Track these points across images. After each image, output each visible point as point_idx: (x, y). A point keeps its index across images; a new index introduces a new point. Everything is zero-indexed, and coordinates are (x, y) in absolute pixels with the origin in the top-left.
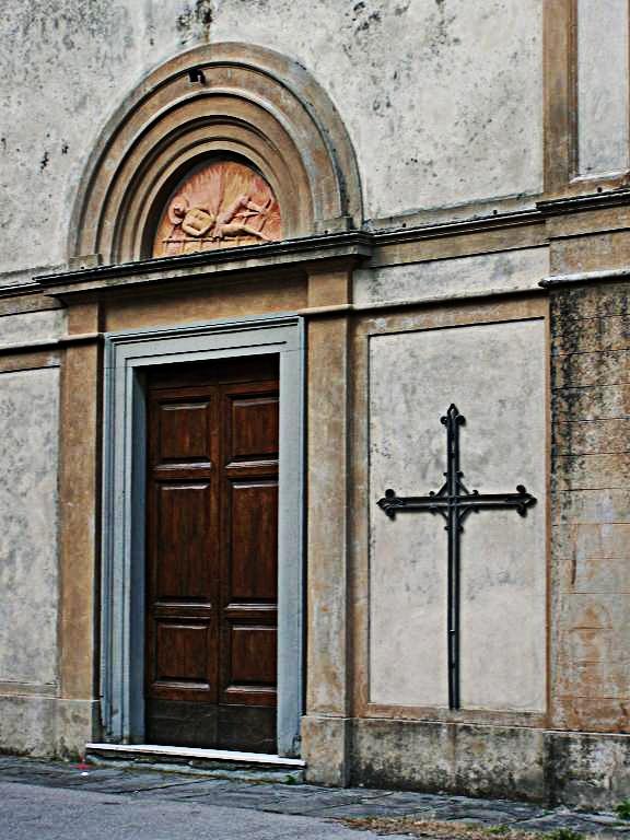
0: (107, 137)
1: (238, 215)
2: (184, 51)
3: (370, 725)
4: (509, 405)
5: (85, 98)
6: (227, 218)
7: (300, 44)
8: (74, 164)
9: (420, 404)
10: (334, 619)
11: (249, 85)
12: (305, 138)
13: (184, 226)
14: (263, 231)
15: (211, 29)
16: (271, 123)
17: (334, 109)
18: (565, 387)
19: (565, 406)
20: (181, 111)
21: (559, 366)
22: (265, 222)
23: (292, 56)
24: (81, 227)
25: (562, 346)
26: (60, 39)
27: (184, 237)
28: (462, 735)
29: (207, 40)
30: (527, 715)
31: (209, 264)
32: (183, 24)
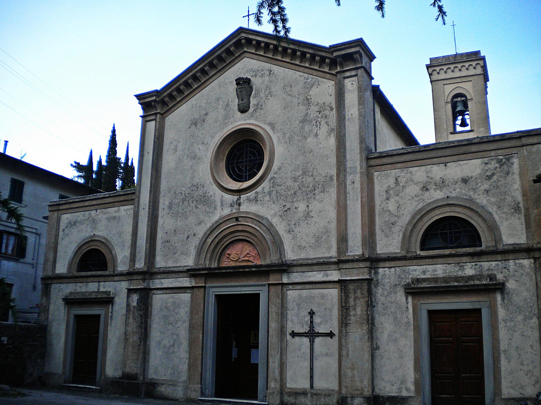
3: (287, 393)
4: (327, 310)
9: (302, 308)
10: (277, 364)
11: (253, 223)
18: (345, 306)
19: (345, 311)
21: (343, 301)
25: (344, 296)
26: (194, 206)
27: (230, 260)
28: (314, 396)
30: (333, 390)
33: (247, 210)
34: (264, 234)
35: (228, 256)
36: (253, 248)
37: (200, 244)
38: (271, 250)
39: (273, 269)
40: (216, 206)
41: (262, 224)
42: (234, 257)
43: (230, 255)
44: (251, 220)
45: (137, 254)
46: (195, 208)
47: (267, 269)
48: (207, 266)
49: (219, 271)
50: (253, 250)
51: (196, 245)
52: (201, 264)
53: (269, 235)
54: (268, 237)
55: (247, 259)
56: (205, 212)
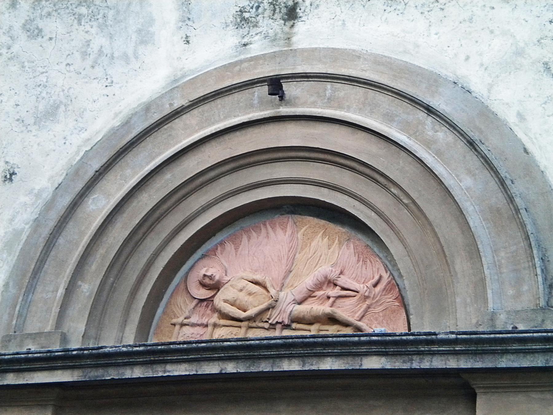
0: (96, 165)
1: (319, 293)
2: (242, 57)
5: (56, 107)
6: (299, 297)
7: (463, 57)
8: (23, 199)
11: (373, 108)
12: (468, 189)
13: (219, 301)
14: (365, 320)
15: (296, 29)
16: (403, 159)
17: (526, 151)
20: (238, 137)
22: (369, 307)
23: (444, 72)
24: (31, 288)
26: (17, 25)
27: (215, 319)
29: (289, 45)
31: (290, 357)
32: (244, 19)
33: (338, 43)
34: (439, 169)
35: (203, 293)
36: (359, 254)
37: (37, 223)
38: (487, 258)
39: (504, 362)
40: (151, 21)
41: (429, 110)
42: (243, 298)
43: (216, 287)
44: (359, 92)
45: (84, 250)
46: (23, 36)
47: (464, 363)
48: (75, 344)
49: (149, 374)
50: (361, 258)
51: (17, 234)
52: (34, 336)
53: (470, 172)
54: (468, 181)
55: (325, 308)
56: (85, 54)
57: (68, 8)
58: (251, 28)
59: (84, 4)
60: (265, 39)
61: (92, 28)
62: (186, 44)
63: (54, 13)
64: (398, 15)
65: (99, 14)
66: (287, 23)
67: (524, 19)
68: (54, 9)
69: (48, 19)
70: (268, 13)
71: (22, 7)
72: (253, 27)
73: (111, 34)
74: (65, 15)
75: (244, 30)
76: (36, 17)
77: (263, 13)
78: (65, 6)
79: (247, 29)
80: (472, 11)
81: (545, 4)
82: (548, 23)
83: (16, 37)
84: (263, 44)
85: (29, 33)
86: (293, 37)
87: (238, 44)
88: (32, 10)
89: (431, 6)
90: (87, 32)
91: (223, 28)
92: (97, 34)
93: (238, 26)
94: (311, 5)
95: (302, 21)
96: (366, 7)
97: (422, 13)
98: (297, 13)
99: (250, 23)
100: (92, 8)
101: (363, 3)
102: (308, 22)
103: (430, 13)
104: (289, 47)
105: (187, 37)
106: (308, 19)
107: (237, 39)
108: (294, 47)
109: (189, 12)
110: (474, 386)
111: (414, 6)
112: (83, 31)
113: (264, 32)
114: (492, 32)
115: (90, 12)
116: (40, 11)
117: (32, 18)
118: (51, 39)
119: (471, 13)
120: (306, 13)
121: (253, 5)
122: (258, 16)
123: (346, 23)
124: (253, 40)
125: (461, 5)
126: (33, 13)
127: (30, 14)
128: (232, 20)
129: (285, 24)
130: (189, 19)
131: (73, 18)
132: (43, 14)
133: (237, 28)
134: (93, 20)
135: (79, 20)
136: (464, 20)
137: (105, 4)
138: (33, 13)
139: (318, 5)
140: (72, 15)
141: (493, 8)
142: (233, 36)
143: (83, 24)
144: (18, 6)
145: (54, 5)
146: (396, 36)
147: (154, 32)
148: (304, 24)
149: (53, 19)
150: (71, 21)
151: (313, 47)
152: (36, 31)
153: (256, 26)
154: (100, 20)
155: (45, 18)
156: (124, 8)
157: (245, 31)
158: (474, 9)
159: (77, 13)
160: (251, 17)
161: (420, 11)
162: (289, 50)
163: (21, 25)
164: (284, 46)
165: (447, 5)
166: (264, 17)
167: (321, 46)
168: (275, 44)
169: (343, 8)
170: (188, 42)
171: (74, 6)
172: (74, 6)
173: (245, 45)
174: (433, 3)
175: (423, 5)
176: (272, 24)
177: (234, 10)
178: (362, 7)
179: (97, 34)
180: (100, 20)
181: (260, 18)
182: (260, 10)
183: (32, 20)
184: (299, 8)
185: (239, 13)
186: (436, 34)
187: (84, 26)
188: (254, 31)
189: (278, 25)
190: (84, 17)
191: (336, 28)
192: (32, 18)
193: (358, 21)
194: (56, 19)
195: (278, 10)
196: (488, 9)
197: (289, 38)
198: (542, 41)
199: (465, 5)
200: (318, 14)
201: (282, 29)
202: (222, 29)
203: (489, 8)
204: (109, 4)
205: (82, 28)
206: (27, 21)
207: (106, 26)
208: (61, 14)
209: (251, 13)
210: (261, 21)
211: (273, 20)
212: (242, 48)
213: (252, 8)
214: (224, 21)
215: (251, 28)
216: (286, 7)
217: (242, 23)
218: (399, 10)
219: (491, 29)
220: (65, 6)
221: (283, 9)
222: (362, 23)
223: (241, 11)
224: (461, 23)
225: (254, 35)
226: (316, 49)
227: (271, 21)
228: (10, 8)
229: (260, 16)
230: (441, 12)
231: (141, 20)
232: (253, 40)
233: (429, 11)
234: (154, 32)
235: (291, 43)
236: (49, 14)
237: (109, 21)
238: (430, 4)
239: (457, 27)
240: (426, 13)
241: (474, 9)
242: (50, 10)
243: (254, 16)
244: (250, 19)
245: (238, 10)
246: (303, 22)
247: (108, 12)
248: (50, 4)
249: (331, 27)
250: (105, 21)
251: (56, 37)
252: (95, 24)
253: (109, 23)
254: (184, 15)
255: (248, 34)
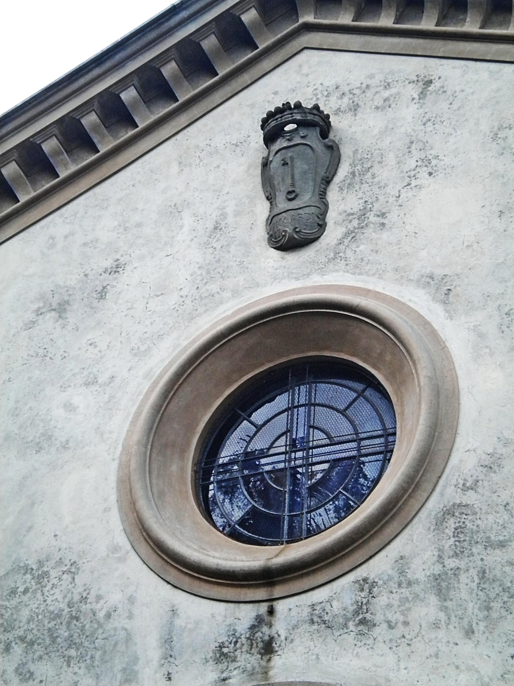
15: (272, 663)
26: (10, 669)
32: (223, 654)
40: (136, 659)
57: (58, 651)
58: (230, 663)
59: (74, 646)
60: (243, 673)
61: (79, 669)
62: (168, 680)
63: (46, 657)
64: (368, 649)
65: (87, 656)
66: (264, 658)
67: (487, 655)
68: (46, 652)
69: (39, 663)
70: (245, 648)
71: (16, 651)
72: (232, 661)
73: (97, 674)
74: (55, 658)
75: (223, 665)
76: (28, 660)
77: (241, 648)
78: (56, 649)
79: (226, 664)
80: (438, 647)
81: (506, 640)
82: (511, 658)
83: (8, 681)
84: (241, 679)
85: (21, 677)
86: (269, 671)
87: (217, 679)
88: (25, 654)
89: (399, 641)
90: (75, 674)
91: (203, 664)
92: (84, 675)
93: (217, 661)
94: (286, 639)
95: (278, 655)
96: (338, 641)
97: (390, 648)
98: (274, 647)
99: (228, 658)
100: (81, 650)
101: (334, 638)
102: (283, 656)
103: (398, 648)
104: (266, 680)
105: (169, 674)
106: (283, 653)
107: (217, 674)
108: (272, 681)
109: (172, 649)
110: (74, 116)
111: (382, 641)
112: (72, 672)
113: (242, 667)
114: (457, 667)
115: (79, 653)
116: (32, 655)
117: (24, 661)
118: (41, 682)
119: (436, 649)
120: (281, 648)
121: (232, 640)
122: (236, 650)
123: (320, 657)
124: (232, 674)
125: (427, 641)
126: (25, 657)
127: (23, 658)
128: (211, 655)
129: (262, 659)
130: (171, 656)
131: (62, 660)
132: (35, 658)
133: (217, 663)
134: (81, 661)
135: (68, 662)
136: (431, 656)
137: (93, 646)
138: (25, 657)
139: (292, 640)
140: (61, 657)
141: (457, 644)
142: (213, 671)
143: (71, 665)
144: (11, 651)
145: (46, 649)
146: (367, 670)
147: (138, 671)
148: (280, 658)
149: (44, 662)
150: (61, 664)
151: (289, 680)
152: (28, 675)
153: (234, 660)
154: (88, 661)
155: (36, 662)
156: (111, 648)
157: (223, 666)
158: (439, 645)
159: (67, 655)
160: (230, 652)
161: (389, 646)
162: (266, 684)
163: (14, 669)
164: (262, 681)
165: (413, 641)
166: (242, 652)
167: (297, 680)
168: (253, 678)
169: (316, 642)
170: (170, 679)
171: (64, 649)
172: (64, 649)
173: (224, 680)
174: (400, 638)
175: (391, 640)
176: (250, 658)
177: (214, 645)
178: (334, 641)
179: (84, 675)
180: (88, 661)
181: (238, 653)
182: (238, 645)
183: (24, 664)
184: (274, 643)
185: (218, 649)
186: (405, 669)
187: (73, 667)
188: (232, 666)
189: (255, 659)
190: (73, 659)
191: (311, 662)
192: (24, 661)
193: (331, 656)
194: (47, 662)
195: (255, 645)
196: (452, 645)
197: (266, 672)
198: (505, 676)
199: (430, 641)
200: (292, 649)
201: (259, 663)
202: (202, 664)
203: (452, 644)
204: (96, 645)
205: (71, 669)
206: (19, 665)
207: (93, 667)
208: (52, 657)
209: (230, 648)
210: (239, 656)
211: (250, 655)
212: (221, 684)
213: (230, 643)
214: (204, 657)
215: (230, 663)
216: (262, 641)
217: (222, 658)
218: (369, 645)
219: (456, 664)
220: (56, 649)
221: (259, 643)
222: (334, 657)
223: (220, 646)
224: (427, 658)
225: (233, 670)
226: (292, 682)
227: (248, 656)
228: (4, 652)
229: (238, 651)
230: (408, 647)
231: (126, 660)
232: (232, 674)
233: (396, 647)
234: (138, 671)
235: (269, 676)
236: (41, 657)
237: (97, 663)
238: (398, 639)
239: (424, 662)
240: (394, 648)
241: (439, 645)
242: (42, 653)
243: (232, 651)
244: (229, 654)
245: (218, 646)
246: (279, 657)
247: (96, 653)
248: (42, 647)
249: (305, 661)
250: (93, 662)
251: (46, 680)
252: (83, 665)
253: (96, 663)
254: (167, 652)
255: (227, 669)
